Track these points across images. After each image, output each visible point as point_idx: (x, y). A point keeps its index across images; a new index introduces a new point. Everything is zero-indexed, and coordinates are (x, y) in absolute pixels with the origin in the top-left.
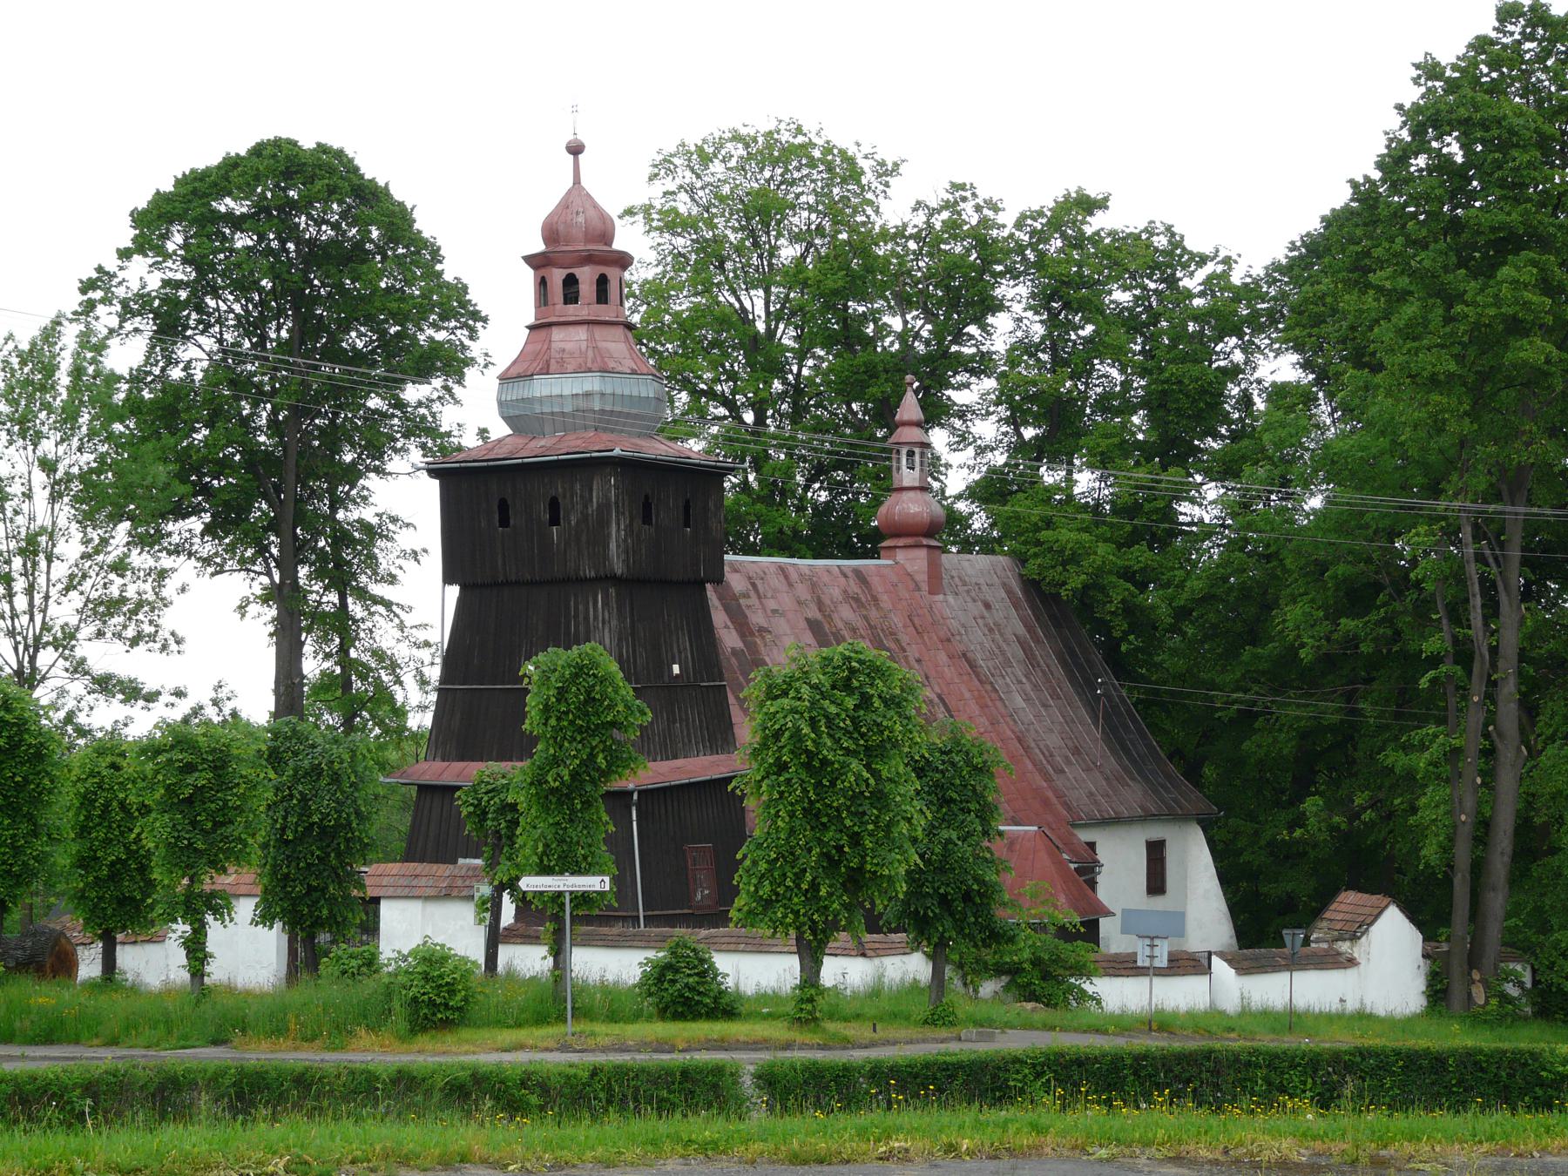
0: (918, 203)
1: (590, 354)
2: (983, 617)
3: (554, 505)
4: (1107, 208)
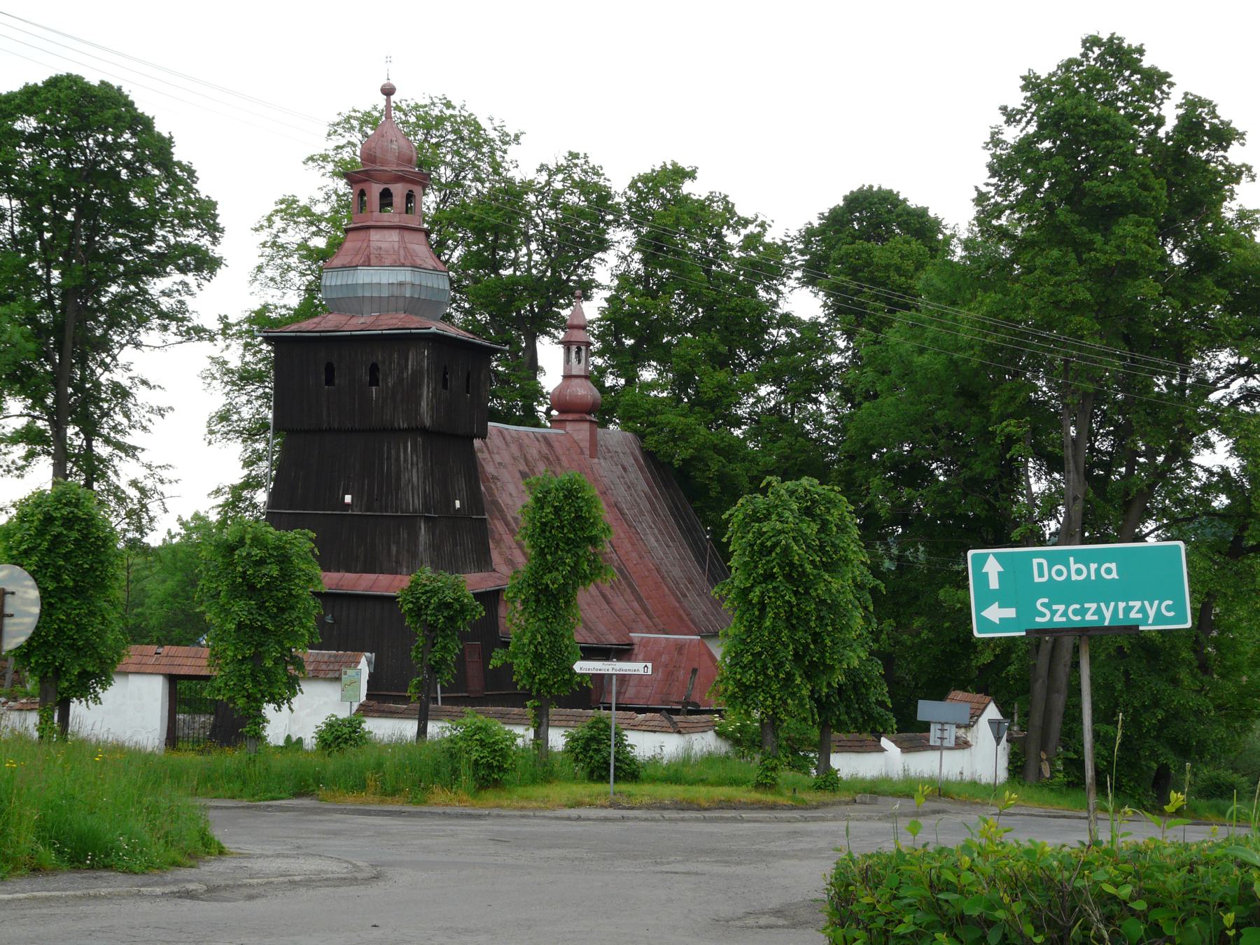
0: (542, 165)
1: (402, 252)
3: (374, 369)
4: (695, 178)
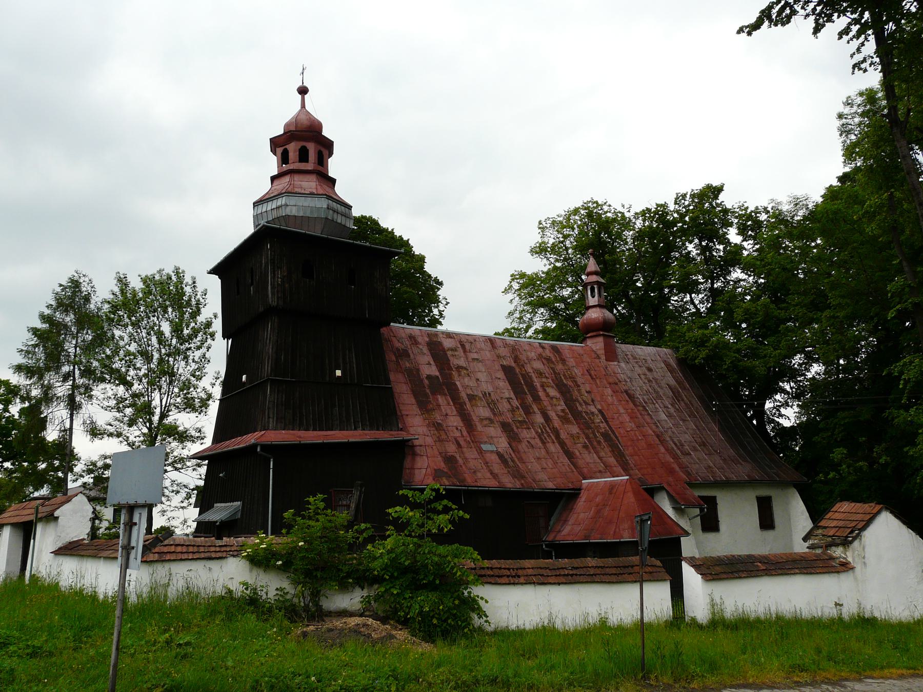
2: (645, 375)
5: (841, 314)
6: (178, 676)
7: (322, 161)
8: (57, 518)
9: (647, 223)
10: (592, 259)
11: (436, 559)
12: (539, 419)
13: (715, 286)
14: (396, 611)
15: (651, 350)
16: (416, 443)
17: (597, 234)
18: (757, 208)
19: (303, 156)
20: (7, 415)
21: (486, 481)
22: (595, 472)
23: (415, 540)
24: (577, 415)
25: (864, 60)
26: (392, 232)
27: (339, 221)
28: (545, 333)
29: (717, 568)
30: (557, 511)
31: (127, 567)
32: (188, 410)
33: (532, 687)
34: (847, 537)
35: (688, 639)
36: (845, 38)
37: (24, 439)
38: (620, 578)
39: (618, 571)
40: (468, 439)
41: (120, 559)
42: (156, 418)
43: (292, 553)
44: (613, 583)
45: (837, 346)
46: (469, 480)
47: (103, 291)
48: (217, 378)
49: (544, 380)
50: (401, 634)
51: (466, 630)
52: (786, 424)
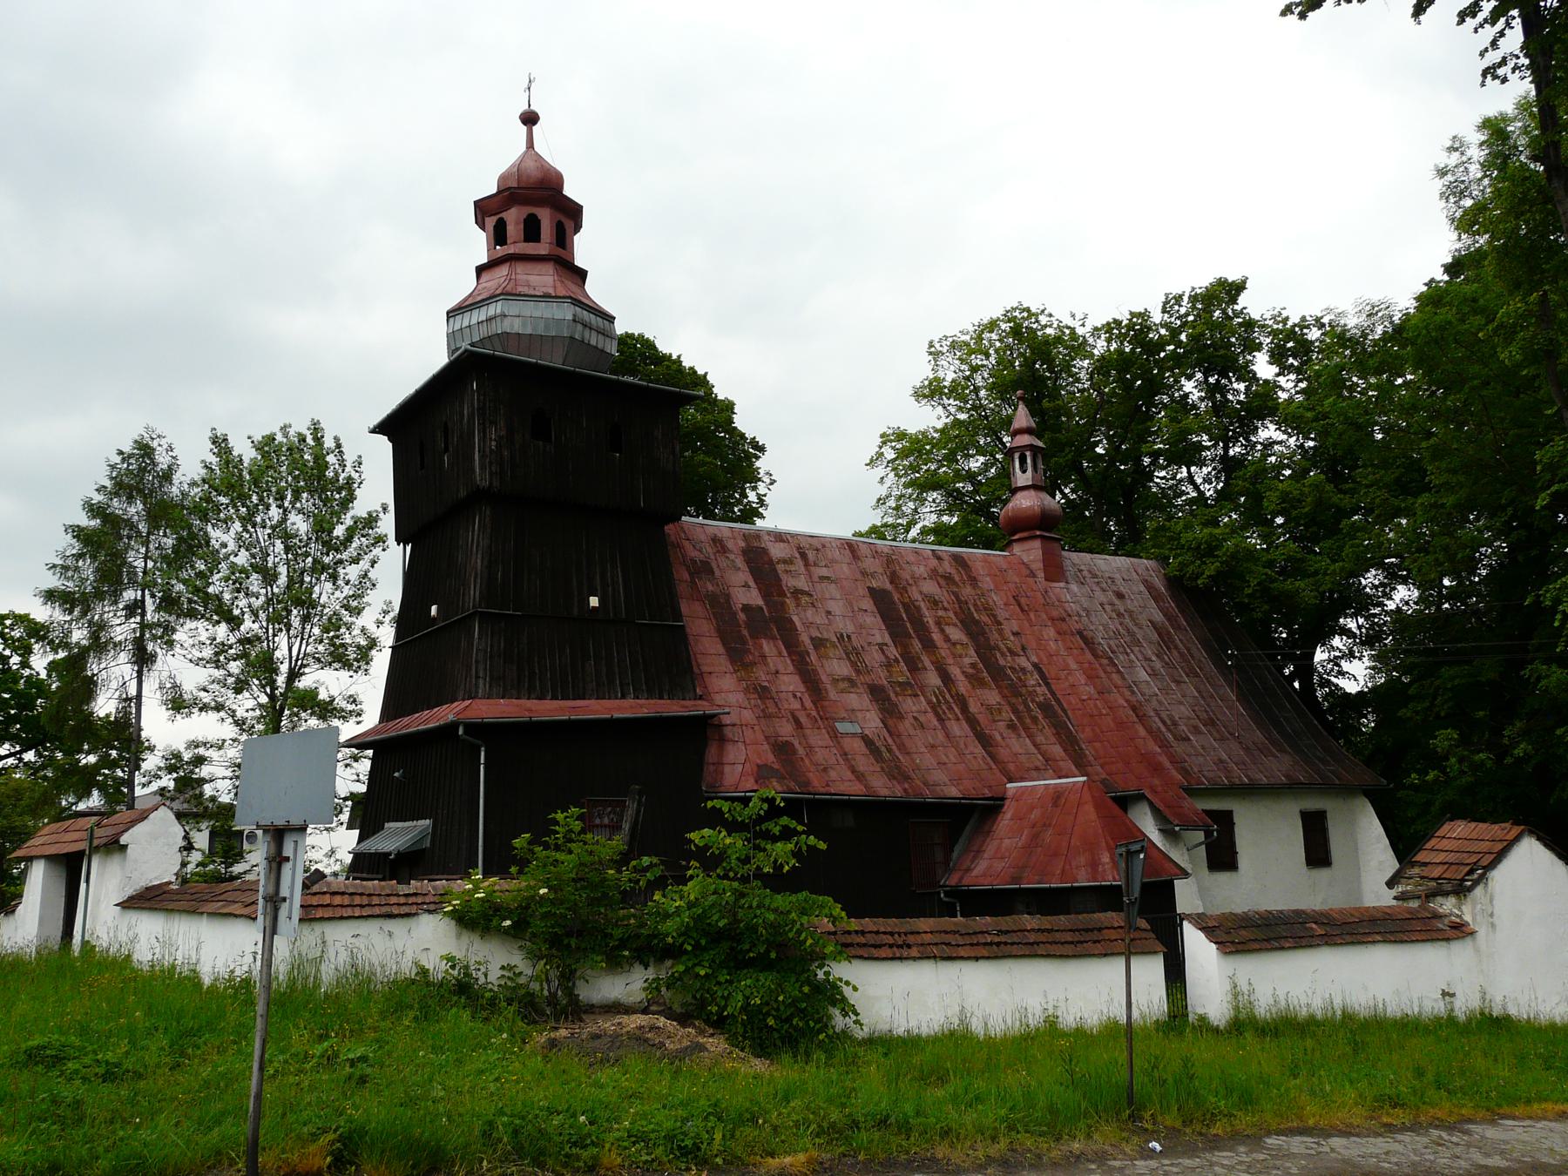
2: (1112, 604)
5: (1449, 500)
6: (356, 1114)
7: (563, 239)
8: (124, 847)
9: (1114, 346)
10: (1021, 407)
11: (771, 917)
12: (933, 679)
13: (1231, 453)
14: (702, 1004)
15: (1121, 562)
16: (726, 720)
17: (1028, 364)
18: (1303, 319)
19: (532, 230)
20: (26, 672)
21: (844, 785)
22: (1028, 770)
23: (736, 884)
24: (998, 674)
25: (1504, 62)
26: (678, 361)
27: (593, 342)
28: (940, 533)
29: (1243, 932)
30: (962, 840)
31: (274, 931)
32: (336, 665)
33: (947, 1133)
34: (1463, 880)
35: (1203, 1053)
36: (1471, 23)
37: (58, 717)
38: (1079, 948)
39: (1077, 937)
40: (814, 713)
41: (260, 918)
42: (281, 680)
43: (527, 907)
44: (1067, 956)
45: (1441, 557)
46: (817, 784)
47: (190, 463)
48: (386, 612)
49: (941, 613)
50: (716, 1044)
51: (821, 1037)
52: (1351, 687)
